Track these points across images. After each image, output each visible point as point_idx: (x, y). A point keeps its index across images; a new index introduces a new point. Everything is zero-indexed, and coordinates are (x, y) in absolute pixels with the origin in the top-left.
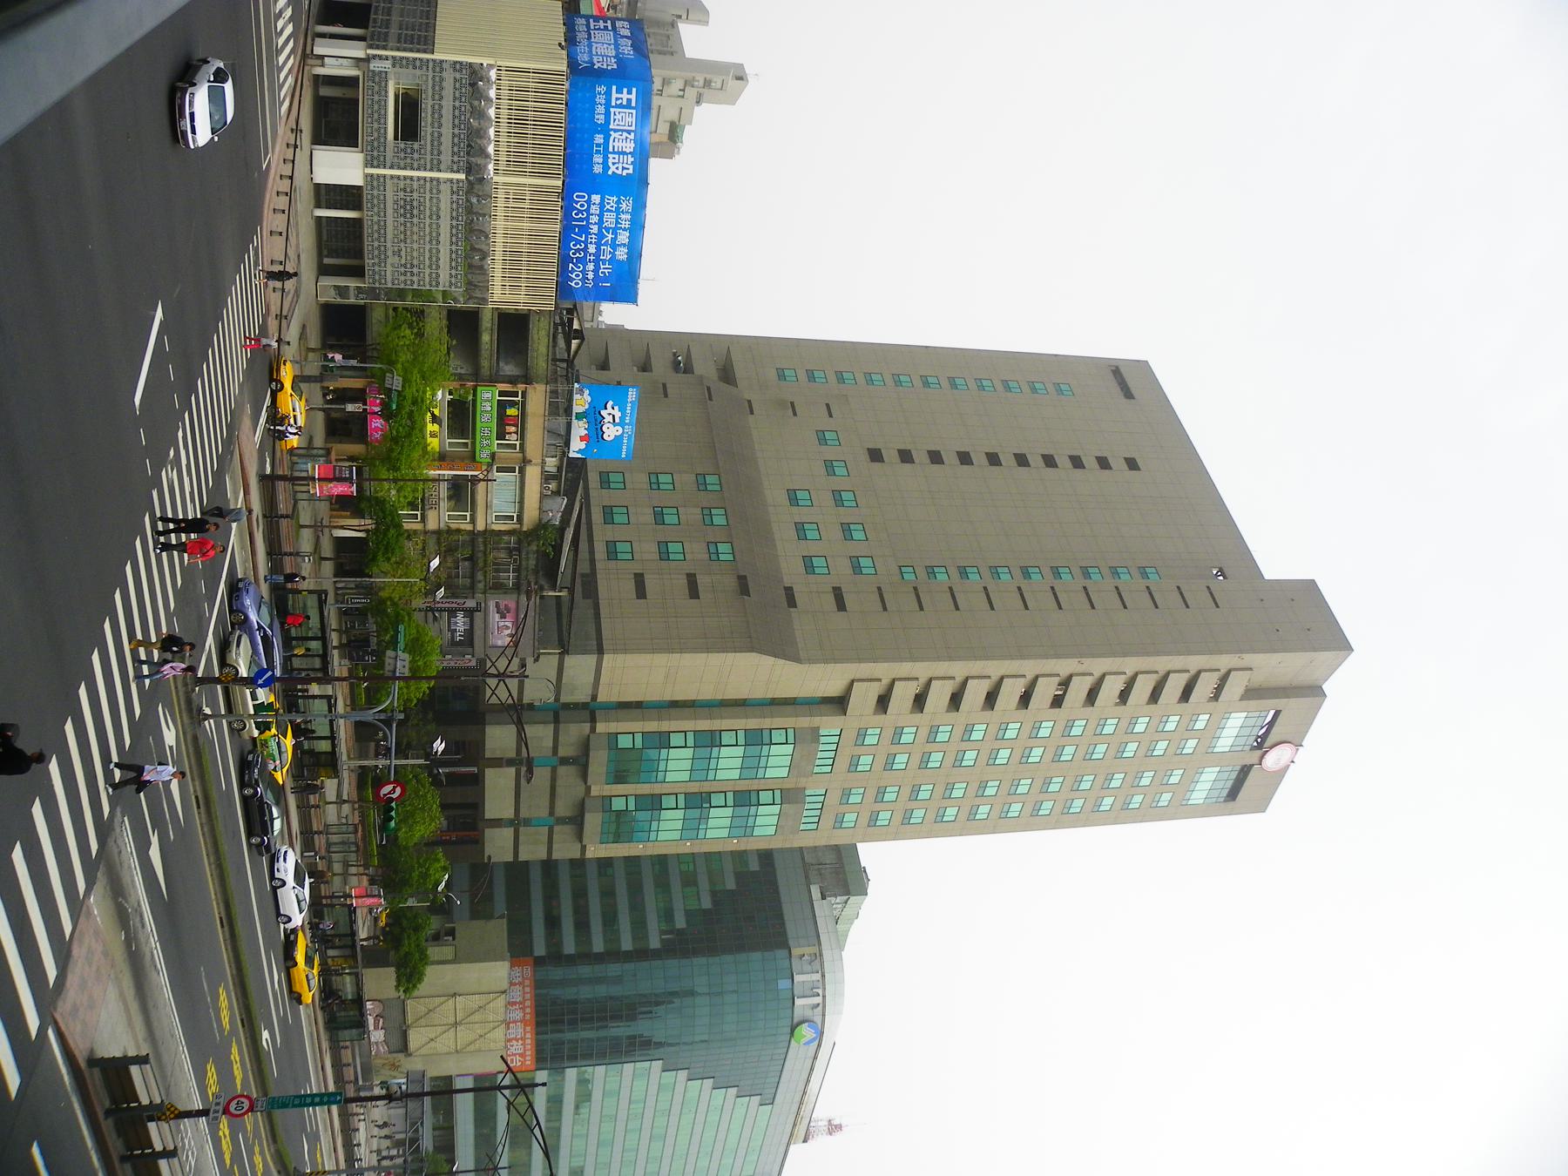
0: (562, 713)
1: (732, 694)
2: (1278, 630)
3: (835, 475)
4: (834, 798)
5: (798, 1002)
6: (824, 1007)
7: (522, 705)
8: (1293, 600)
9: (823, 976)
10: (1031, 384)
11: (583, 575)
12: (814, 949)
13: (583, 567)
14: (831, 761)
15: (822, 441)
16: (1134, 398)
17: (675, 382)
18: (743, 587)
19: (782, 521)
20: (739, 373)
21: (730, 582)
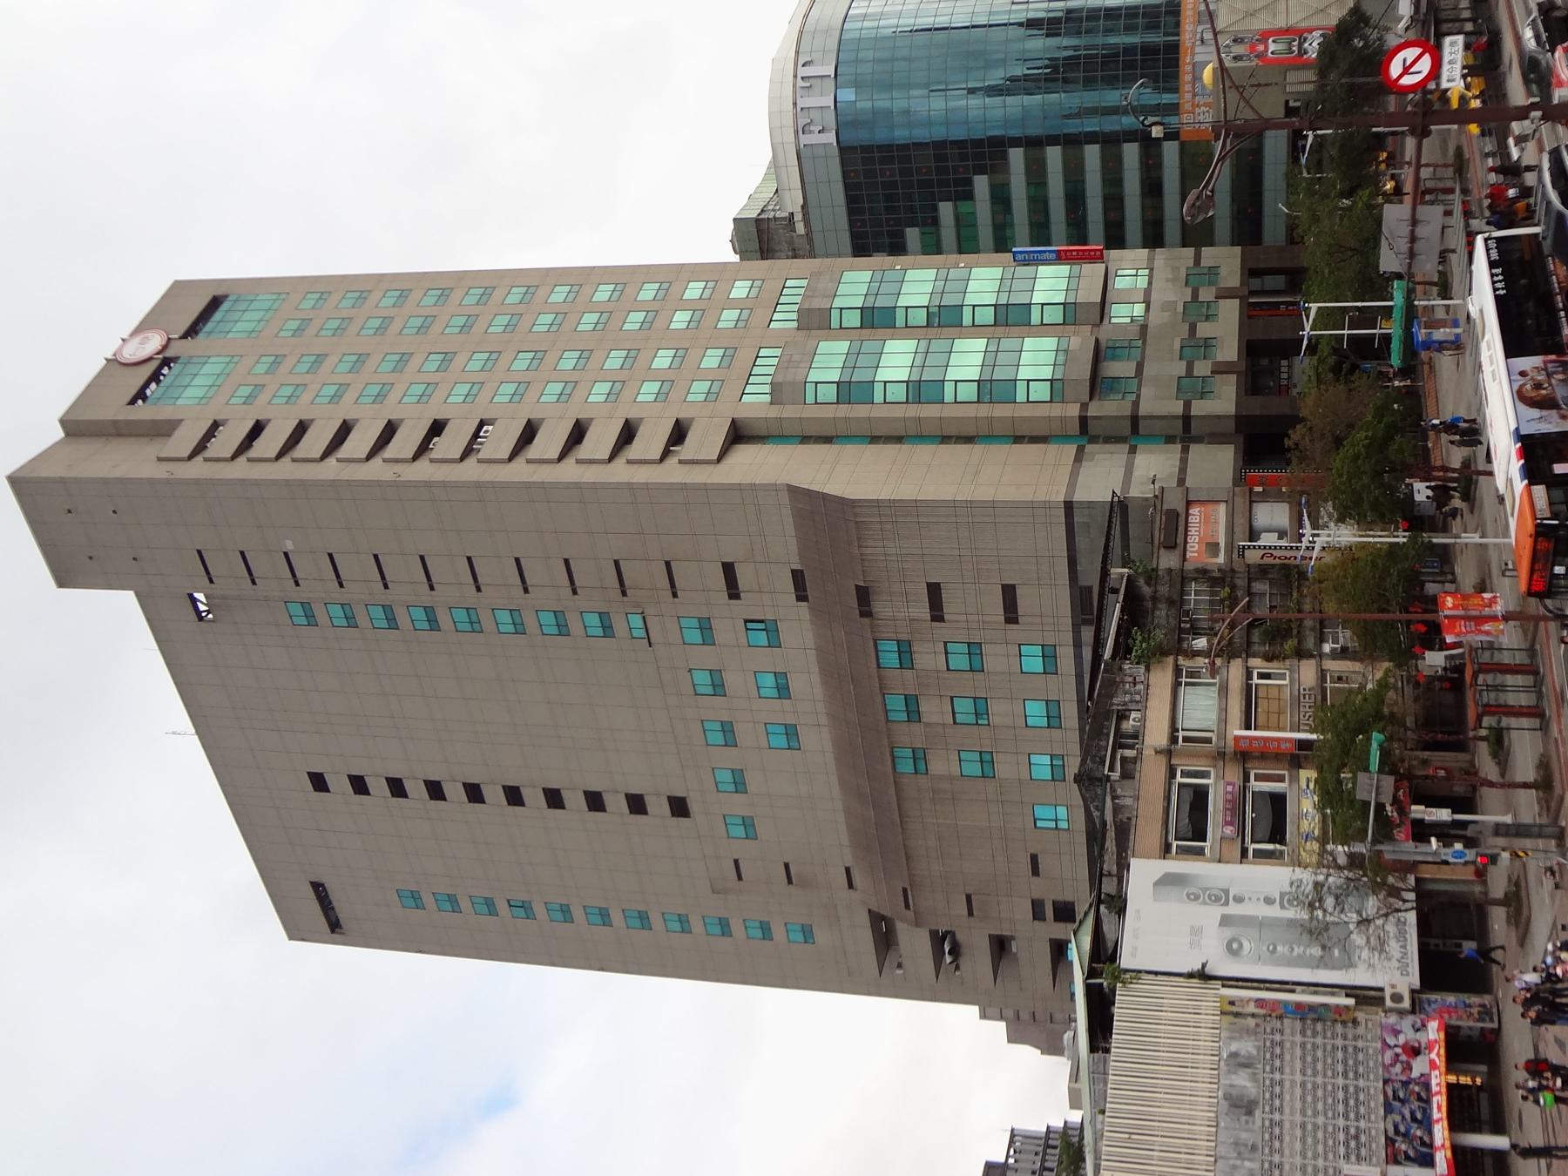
0: (1127, 431)
1: (890, 450)
2: (114, 512)
3: (733, 770)
5: (830, 70)
6: (796, 64)
7: (1183, 440)
9: (795, 104)
13: (1088, 634)
15: (748, 823)
16: (311, 883)
17: (952, 915)
18: (864, 596)
19: (808, 683)
20: (865, 938)
21: (881, 607)
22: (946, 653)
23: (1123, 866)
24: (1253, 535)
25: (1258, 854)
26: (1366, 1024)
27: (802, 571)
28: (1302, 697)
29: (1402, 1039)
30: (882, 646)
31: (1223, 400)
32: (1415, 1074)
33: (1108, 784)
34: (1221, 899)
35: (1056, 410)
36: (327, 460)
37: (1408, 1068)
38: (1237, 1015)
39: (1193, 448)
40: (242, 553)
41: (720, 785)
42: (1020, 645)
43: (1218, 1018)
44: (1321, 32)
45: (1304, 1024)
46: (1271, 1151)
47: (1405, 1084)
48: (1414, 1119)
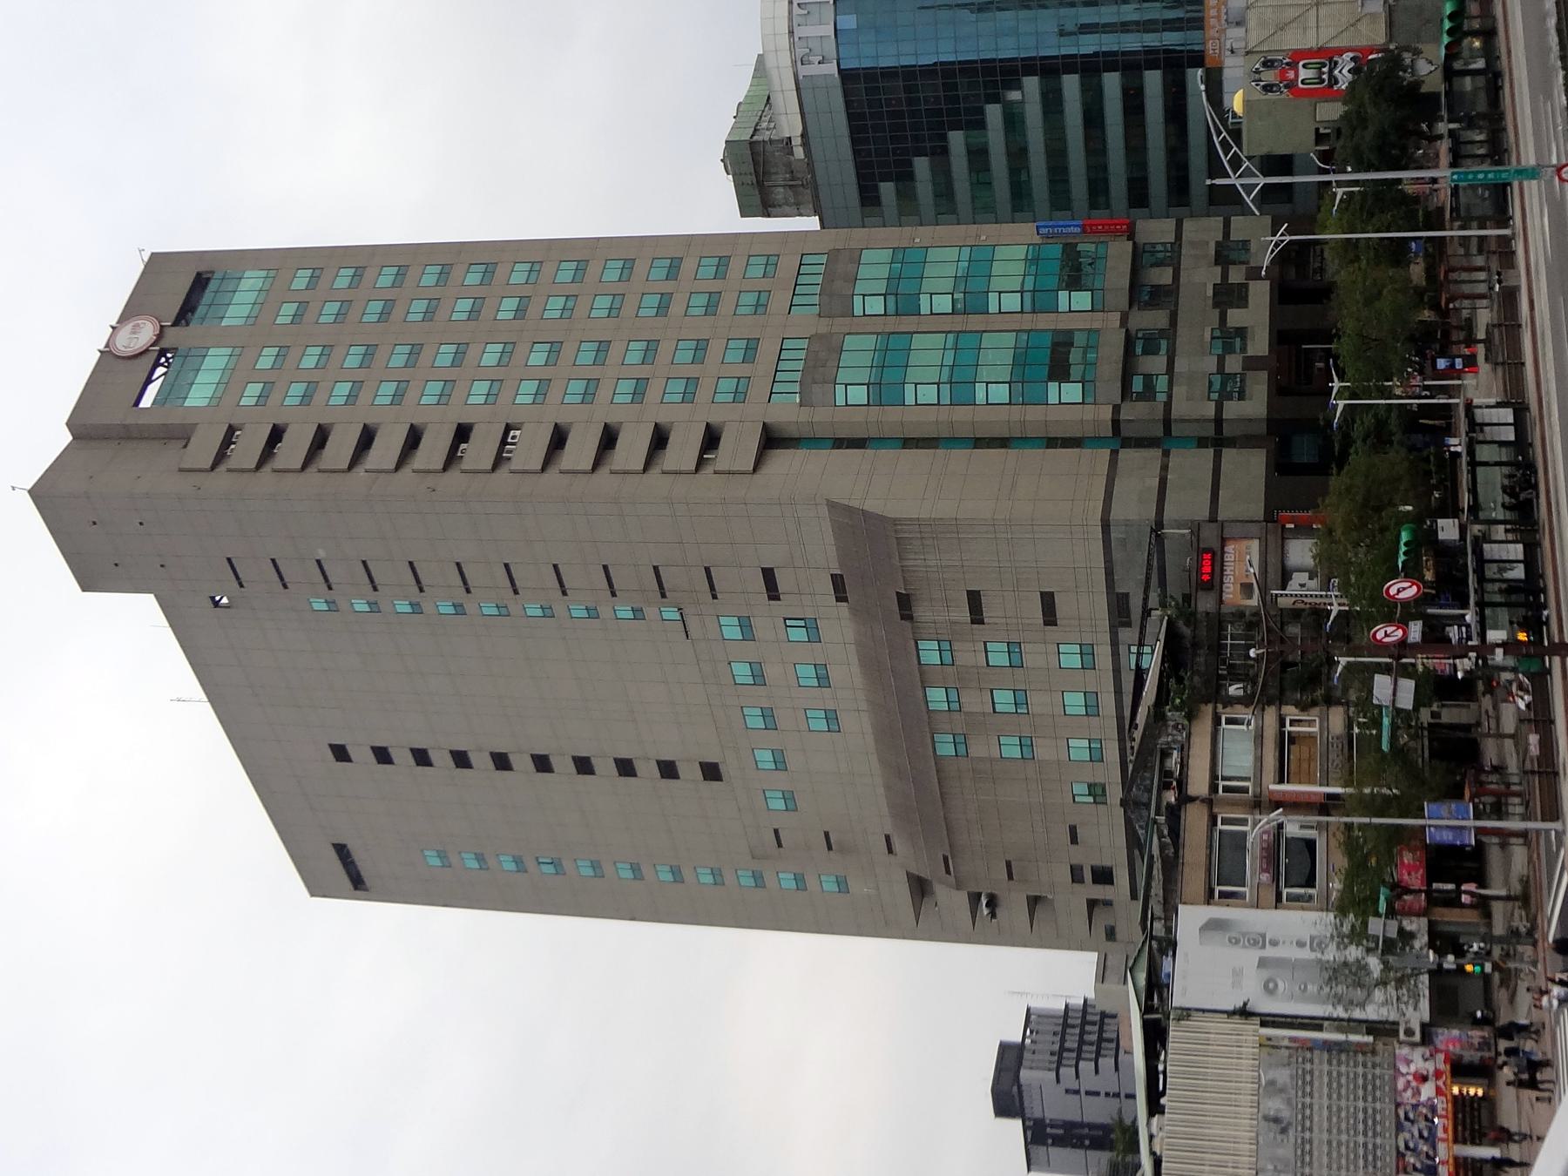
0: (1159, 432)
2: (141, 524)
4: (780, 300)
8: (116, 565)
9: (791, 33)
10: (484, 867)
11: (1128, 624)
12: (804, 71)
14: (785, 355)
16: (333, 845)
18: (905, 604)
19: (848, 672)
20: (903, 891)
21: (922, 612)
22: (986, 652)
23: (1170, 911)
24: (1285, 577)
25: (1291, 898)
26: (1383, 1054)
27: (841, 576)
28: (1330, 745)
29: (1413, 1068)
30: (922, 644)
31: (1254, 405)
32: (1423, 1098)
33: (1155, 826)
34: (1258, 943)
35: (1089, 413)
36: (354, 470)
37: (1417, 1092)
38: (1273, 1047)
39: (1225, 451)
40: (273, 561)
41: (759, 764)
42: (1058, 644)
43: (1257, 1050)
44: (1351, 55)
45: (1330, 1055)
46: (1303, 1060)
47: (1415, 1107)
48: (1421, 1136)
